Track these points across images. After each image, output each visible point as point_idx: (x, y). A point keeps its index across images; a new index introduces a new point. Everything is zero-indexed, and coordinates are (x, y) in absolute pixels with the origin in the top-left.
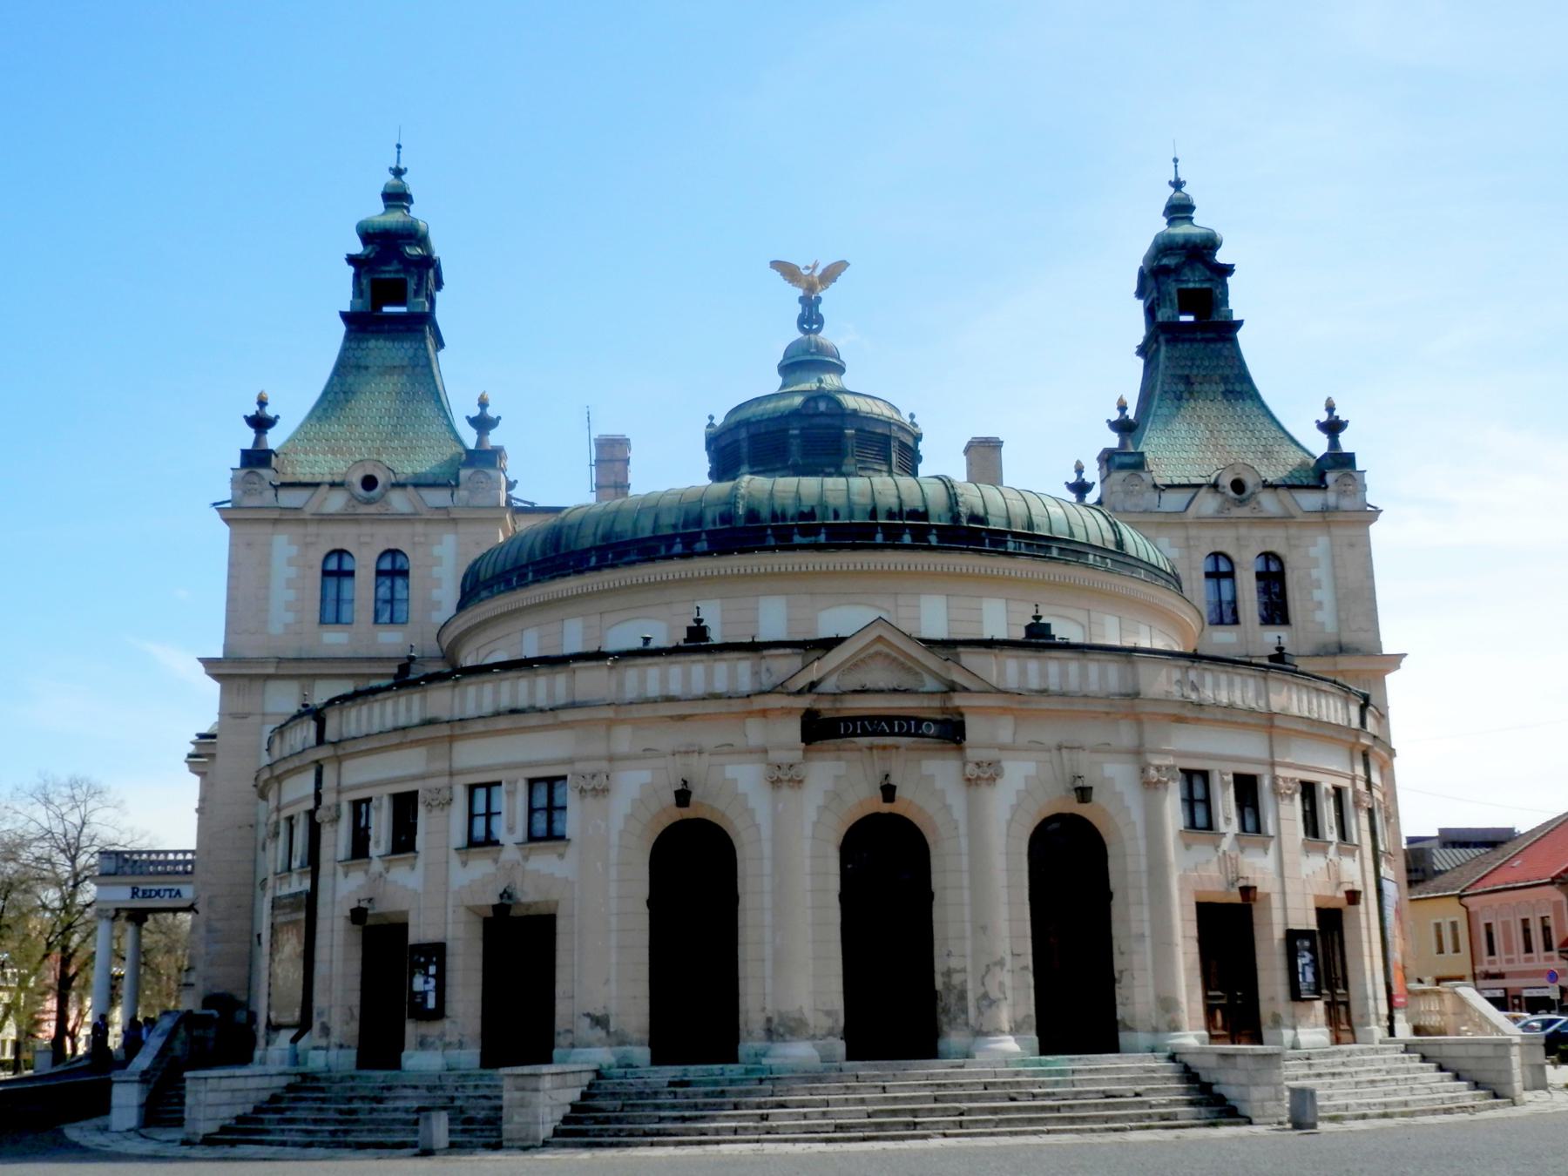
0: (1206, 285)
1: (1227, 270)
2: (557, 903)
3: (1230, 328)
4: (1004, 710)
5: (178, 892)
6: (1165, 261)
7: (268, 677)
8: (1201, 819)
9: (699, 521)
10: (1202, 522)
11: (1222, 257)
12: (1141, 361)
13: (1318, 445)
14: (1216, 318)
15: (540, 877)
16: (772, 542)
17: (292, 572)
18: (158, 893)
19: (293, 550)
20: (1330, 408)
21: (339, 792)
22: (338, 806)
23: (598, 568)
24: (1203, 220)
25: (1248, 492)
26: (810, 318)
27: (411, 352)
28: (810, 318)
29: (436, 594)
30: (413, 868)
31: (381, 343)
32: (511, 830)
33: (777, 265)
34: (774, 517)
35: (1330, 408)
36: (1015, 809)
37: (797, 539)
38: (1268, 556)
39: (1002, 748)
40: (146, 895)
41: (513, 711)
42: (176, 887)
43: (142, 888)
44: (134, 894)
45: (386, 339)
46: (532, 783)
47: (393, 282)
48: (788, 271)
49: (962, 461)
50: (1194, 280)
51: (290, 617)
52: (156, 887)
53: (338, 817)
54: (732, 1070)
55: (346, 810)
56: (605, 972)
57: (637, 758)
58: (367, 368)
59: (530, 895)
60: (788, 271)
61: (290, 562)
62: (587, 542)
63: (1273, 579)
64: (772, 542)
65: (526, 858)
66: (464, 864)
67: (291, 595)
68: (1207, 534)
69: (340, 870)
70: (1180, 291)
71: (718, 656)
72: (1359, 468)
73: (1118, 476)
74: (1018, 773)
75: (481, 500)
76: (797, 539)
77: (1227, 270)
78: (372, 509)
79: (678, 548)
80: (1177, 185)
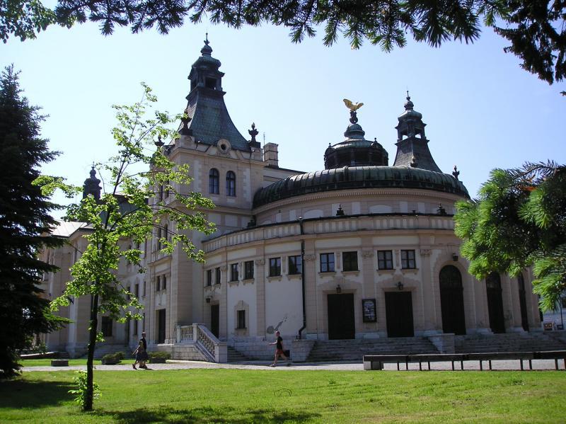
1: (222, 74)
3: (221, 94)
4: (432, 234)
6: (201, 67)
9: (399, 177)
11: (220, 69)
12: (187, 101)
15: (410, 278)
16: (421, 186)
17: (200, 174)
19: (200, 166)
20: (253, 127)
21: (264, 255)
23: (365, 188)
24: (214, 55)
26: (354, 118)
28: (354, 118)
29: (245, 188)
30: (253, 283)
32: (339, 267)
33: (345, 100)
34: (420, 179)
35: (253, 127)
36: (436, 263)
37: (427, 187)
38: (230, 173)
39: (432, 246)
41: (395, 229)
48: (348, 103)
49: (486, 177)
50: (211, 76)
54: (413, 338)
56: (427, 308)
57: (437, 246)
59: (346, 289)
60: (348, 103)
61: (200, 171)
62: (361, 179)
63: (231, 177)
64: (403, 185)
65: (404, 274)
66: (270, 281)
69: (228, 285)
70: (206, 78)
71: (391, 217)
74: (436, 253)
75: (257, 158)
76: (427, 187)
77: (222, 74)
78: (224, 156)
79: (394, 185)
80: (207, 42)
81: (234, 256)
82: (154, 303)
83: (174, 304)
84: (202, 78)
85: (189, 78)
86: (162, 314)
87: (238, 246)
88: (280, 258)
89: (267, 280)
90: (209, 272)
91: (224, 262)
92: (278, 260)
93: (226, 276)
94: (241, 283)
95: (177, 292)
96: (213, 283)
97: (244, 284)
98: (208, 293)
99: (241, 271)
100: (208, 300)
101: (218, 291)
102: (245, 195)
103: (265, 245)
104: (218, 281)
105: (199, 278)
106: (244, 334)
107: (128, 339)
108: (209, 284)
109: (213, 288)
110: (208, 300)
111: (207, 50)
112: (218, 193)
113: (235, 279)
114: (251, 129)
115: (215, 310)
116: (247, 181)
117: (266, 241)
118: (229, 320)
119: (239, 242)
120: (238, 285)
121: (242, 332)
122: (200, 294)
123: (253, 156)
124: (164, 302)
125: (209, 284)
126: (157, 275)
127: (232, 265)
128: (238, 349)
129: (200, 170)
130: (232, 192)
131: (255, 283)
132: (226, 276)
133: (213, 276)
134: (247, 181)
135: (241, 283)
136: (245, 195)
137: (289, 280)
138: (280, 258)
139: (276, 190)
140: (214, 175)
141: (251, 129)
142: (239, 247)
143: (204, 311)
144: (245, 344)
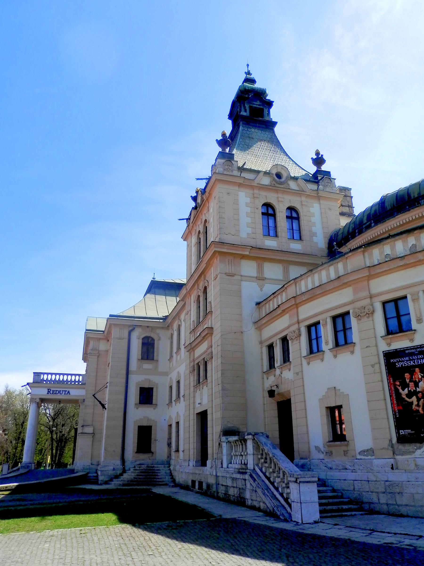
0: (262, 107)
2: (289, 392)
5: (69, 392)
7: (243, 257)
8: (341, 340)
10: (262, 187)
13: (313, 169)
14: (266, 118)
18: (59, 392)
19: (248, 200)
22: (299, 329)
25: (283, 180)
27: (269, 136)
29: (314, 229)
30: (352, 352)
31: (256, 130)
38: (291, 209)
40: (54, 393)
42: (68, 390)
43: (52, 389)
44: (49, 392)
45: (258, 130)
46: (334, 318)
47: (251, 111)
50: (257, 104)
51: (249, 230)
52: (59, 390)
53: (300, 335)
55: (304, 331)
58: (253, 138)
63: (293, 214)
67: (249, 220)
68: (264, 193)
72: (235, 159)
73: (221, 161)
81: (308, 312)
82: (194, 403)
83: (218, 401)
84: (245, 108)
86: (203, 416)
87: (313, 294)
88: (405, 297)
89: (304, 362)
90: (271, 347)
91: (294, 324)
92: (400, 303)
93: (299, 347)
94: (328, 355)
95: (220, 382)
96: (277, 364)
97: (335, 356)
98: (270, 382)
99: (327, 333)
100: (271, 393)
101: (288, 375)
102: (315, 239)
103: (370, 277)
104: (286, 358)
105: (257, 357)
106: (346, 453)
107: (169, 456)
108: (272, 366)
109: (278, 372)
110: (271, 393)
112: (276, 236)
113: (341, 340)
114: (315, 157)
115: (284, 409)
116: (316, 219)
117: (373, 271)
118: (311, 427)
119: (317, 284)
120: (322, 360)
121: (339, 446)
122: (258, 384)
123: (321, 187)
124: (205, 401)
125: (272, 366)
126: (196, 362)
127: (309, 328)
128: (337, 486)
129: (247, 205)
130: (297, 234)
131: (357, 349)
132: (299, 347)
133: (278, 353)
134: (316, 219)
135: (328, 355)
136: (315, 239)
137: (335, 356)
138: (405, 297)
139: (365, 218)
140: (269, 211)
141: (315, 157)
142: (318, 291)
143: (265, 418)
144: (351, 476)
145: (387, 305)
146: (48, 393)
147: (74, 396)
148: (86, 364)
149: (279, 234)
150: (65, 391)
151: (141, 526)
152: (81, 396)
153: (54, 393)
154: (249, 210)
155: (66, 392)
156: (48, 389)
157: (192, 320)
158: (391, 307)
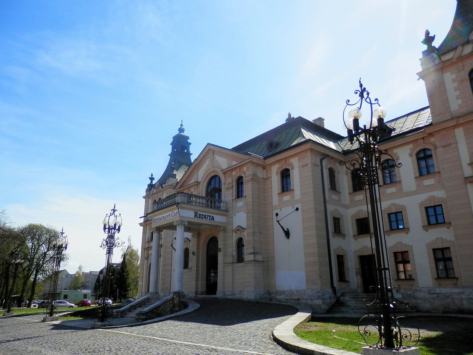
1: (190, 144)
5: (213, 218)
18: (205, 216)
40: (201, 216)
42: (212, 215)
43: (199, 213)
44: (196, 216)
51: (460, 101)
52: (205, 214)
77: (190, 144)
85: (171, 144)
111: (181, 130)
145: (429, 209)
146: (195, 217)
147: (217, 222)
148: (142, 227)
149: (448, 246)
150: (210, 216)
151: (454, 81)
152: (222, 223)
153: (201, 216)
154: (456, 85)
155: (211, 218)
156: (195, 213)
157: (147, 237)
158: (431, 212)
